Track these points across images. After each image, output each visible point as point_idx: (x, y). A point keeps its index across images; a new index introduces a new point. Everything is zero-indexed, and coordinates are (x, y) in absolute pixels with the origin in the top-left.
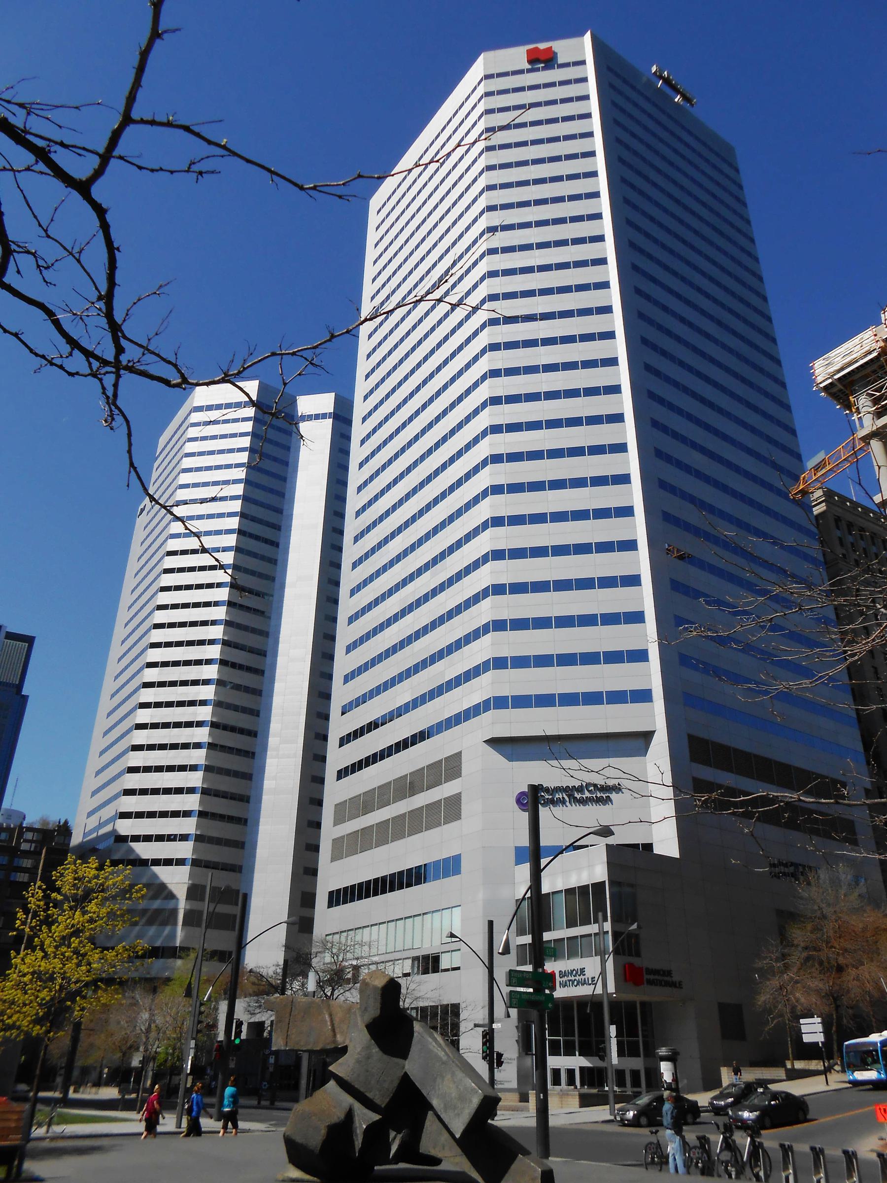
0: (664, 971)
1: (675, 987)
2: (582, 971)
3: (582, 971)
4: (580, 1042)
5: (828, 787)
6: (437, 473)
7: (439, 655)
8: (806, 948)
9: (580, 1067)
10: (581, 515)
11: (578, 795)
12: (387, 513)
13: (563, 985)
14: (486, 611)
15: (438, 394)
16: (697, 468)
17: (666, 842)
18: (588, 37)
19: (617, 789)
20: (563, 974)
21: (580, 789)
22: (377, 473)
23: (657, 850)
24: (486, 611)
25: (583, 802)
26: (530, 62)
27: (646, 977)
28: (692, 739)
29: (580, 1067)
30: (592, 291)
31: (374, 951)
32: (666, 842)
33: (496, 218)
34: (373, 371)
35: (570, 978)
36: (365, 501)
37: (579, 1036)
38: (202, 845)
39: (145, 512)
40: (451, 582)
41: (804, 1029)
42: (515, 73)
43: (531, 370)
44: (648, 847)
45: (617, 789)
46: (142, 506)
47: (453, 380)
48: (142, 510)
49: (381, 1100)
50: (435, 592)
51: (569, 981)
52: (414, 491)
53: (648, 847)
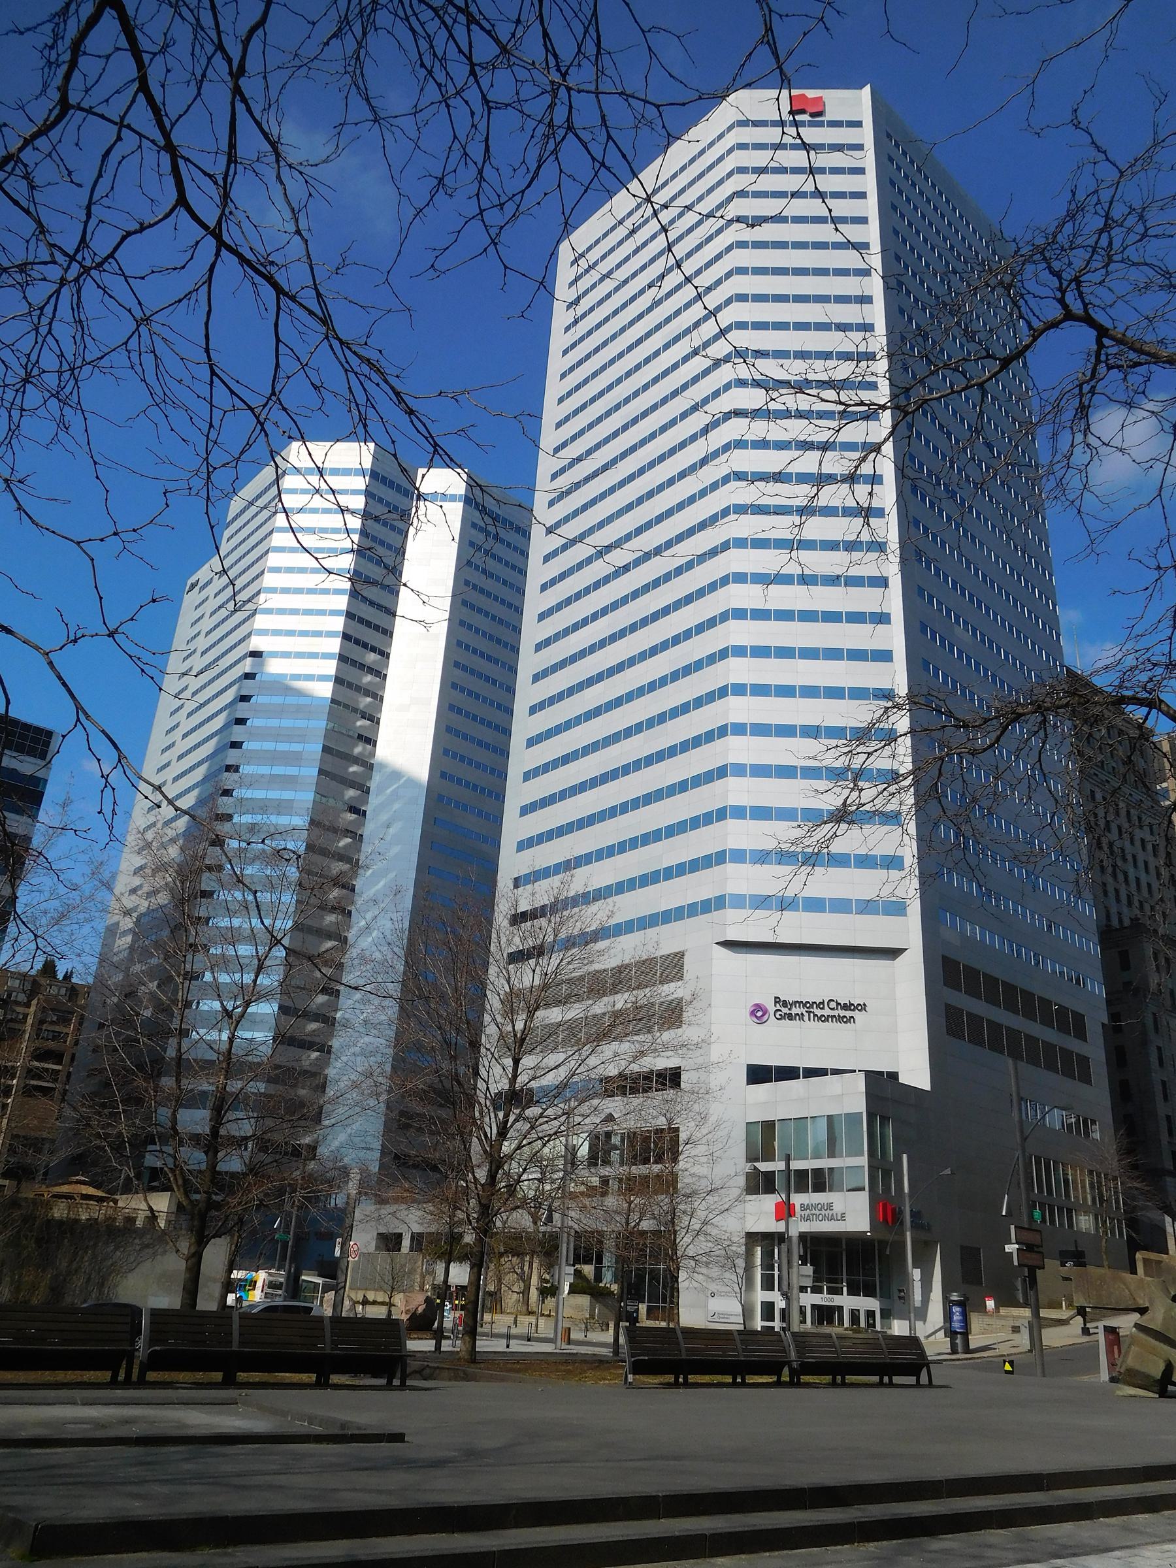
3: (830, 1206)
5: (1075, 1024)
6: (655, 617)
7: (656, 836)
9: (813, 1306)
10: (834, 654)
11: (819, 1012)
12: (583, 654)
15: (659, 519)
16: (988, 971)
17: (916, 1072)
18: (868, 88)
19: (863, 1007)
21: (820, 1005)
22: (570, 572)
23: (902, 1080)
25: (824, 1019)
28: (945, 959)
29: (813, 1306)
30: (852, 267)
32: (916, 1072)
33: (741, 258)
34: (572, 369)
35: (813, 1212)
36: (555, 573)
38: (329, 757)
39: (197, 588)
40: (672, 751)
43: (786, 691)
44: (894, 1076)
45: (863, 1007)
46: (193, 580)
47: (681, 506)
48: (193, 586)
50: (649, 761)
52: (622, 633)
53: (894, 1076)
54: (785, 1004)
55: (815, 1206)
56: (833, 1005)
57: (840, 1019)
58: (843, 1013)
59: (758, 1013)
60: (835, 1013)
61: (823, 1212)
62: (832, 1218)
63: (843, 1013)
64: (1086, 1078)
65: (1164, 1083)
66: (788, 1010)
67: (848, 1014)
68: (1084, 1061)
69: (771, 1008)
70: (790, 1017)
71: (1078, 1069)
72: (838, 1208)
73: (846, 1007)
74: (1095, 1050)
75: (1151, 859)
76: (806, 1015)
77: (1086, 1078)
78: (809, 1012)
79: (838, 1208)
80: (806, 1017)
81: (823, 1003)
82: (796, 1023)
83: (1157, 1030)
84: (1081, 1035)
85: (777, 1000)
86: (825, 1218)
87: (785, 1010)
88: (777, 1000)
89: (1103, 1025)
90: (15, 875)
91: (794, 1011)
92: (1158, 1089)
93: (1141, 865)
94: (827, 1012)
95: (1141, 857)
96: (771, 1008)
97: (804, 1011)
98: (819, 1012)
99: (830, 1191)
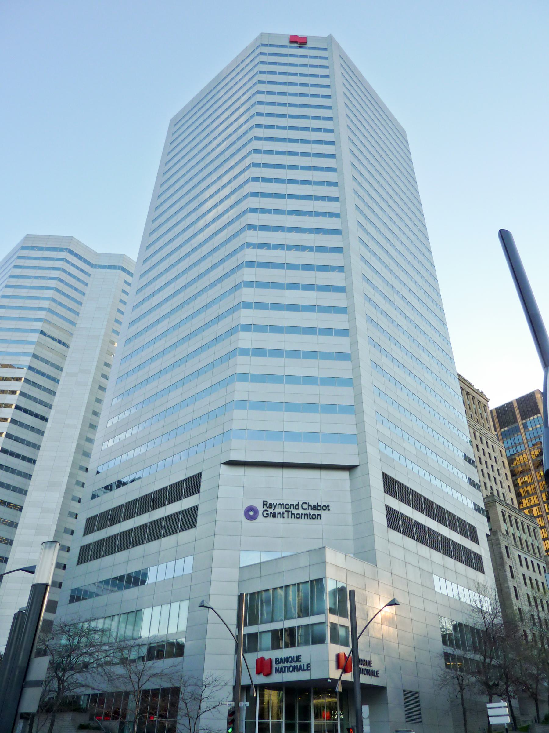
0: (293, 658)
1: (374, 675)
2: (298, 658)
3: (298, 658)
4: (286, 724)
8: (108, 589)
13: (279, 671)
14: (58, 264)
19: (327, 508)
20: (278, 661)
21: (296, 507)
24: (58, 264)
25: (298, 516)
26: (291, 42)
27: (274, 666)
31: (105, 640)
35: (286, 664)
37: (286, 719)
41: (490, 712)
42: (281, 46)
45: (327, 508)
49: (489, 710)
51: (285, 667)
54: (271, 506)
55: (287, 660)
56: (305, 506)
57: (311, 517)
58: (312, 512)
59: (251, 513)
60: (307, 512)
61: (293, 664)
62: (300, 669)
63: (312, 512)
64: (480, 569)
65: (515, 588)
66: (86, 273)
67: (316, 512)
68: (479, 558)
69: (261, 509)
70: (274, 515)
71: (473, 561)
72: (304, 661)
73: (315, 508)
74: (482, 549)
75: (494, 464)
76: (286, 514)
77: (480, 569)
78: (288, 512)
79: (304, 661)
80: (286, 514)
81: (298, 505)
82: (279, 520)
83: (508, 556)
84: (475, 539)
85: (265, 503)
86: (295, 669)
87: (271, 510)
88: (265, 503)
89: (487, 535)
90: (356, 694)
91: (277, 511)
92: (512, 591)
93: (490, 467)
94: (301, 511)
95: (489, 463)
96: (261, 509)
97: (284, 510)
98: (295, 512)
99: (298, 646)
